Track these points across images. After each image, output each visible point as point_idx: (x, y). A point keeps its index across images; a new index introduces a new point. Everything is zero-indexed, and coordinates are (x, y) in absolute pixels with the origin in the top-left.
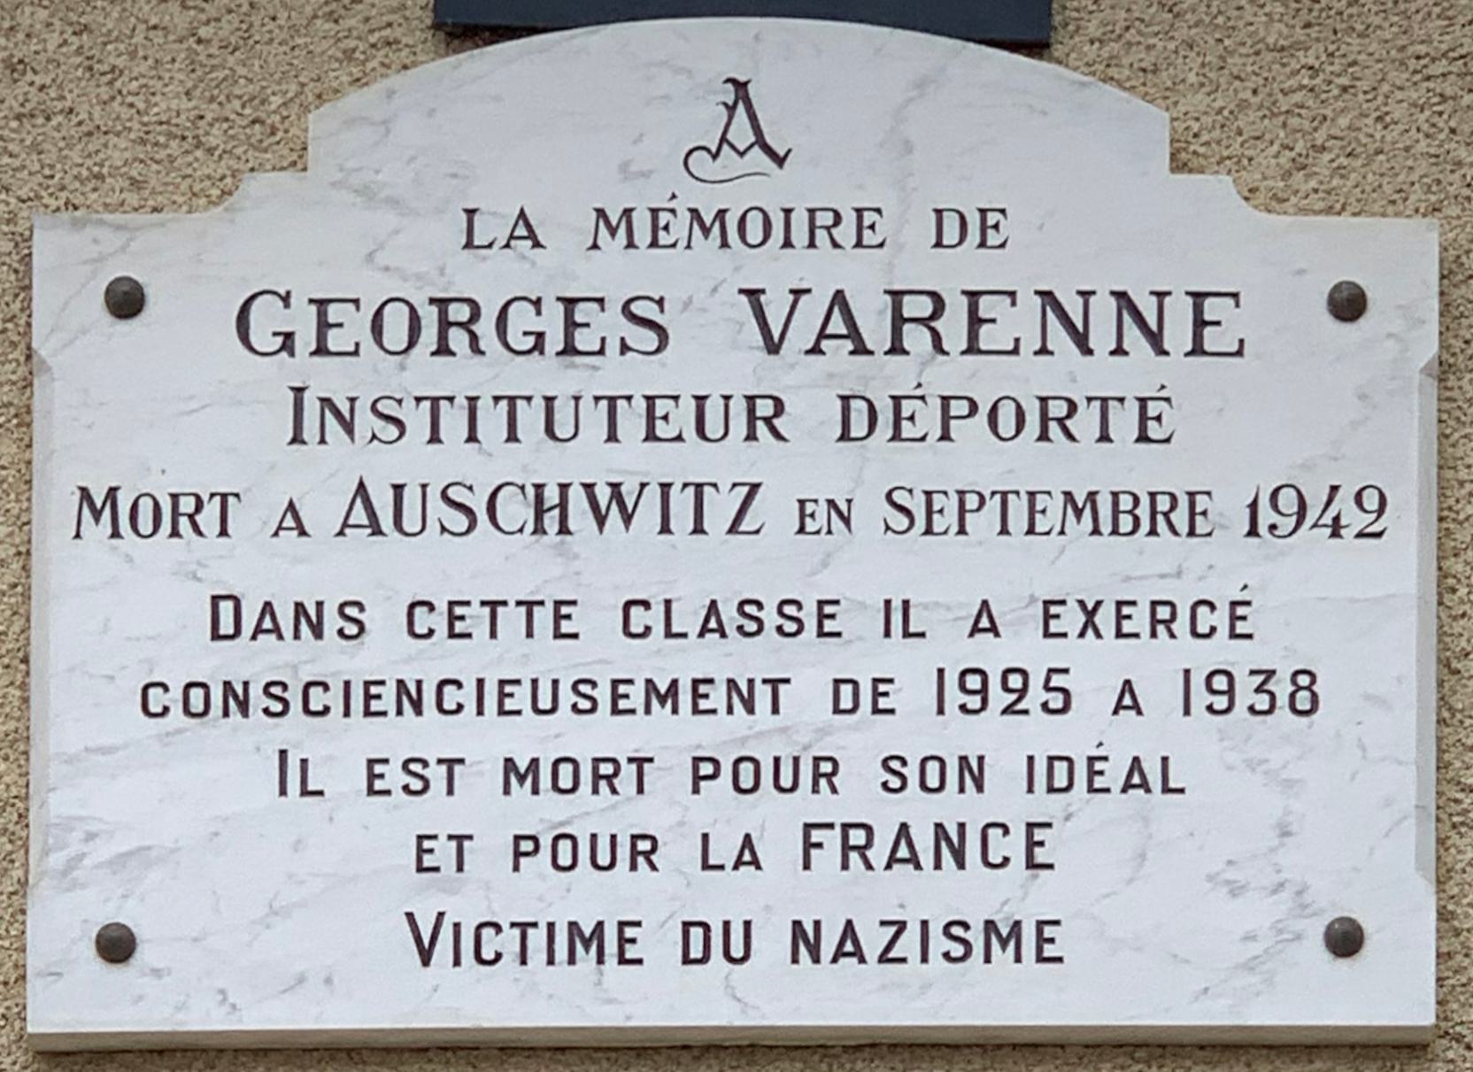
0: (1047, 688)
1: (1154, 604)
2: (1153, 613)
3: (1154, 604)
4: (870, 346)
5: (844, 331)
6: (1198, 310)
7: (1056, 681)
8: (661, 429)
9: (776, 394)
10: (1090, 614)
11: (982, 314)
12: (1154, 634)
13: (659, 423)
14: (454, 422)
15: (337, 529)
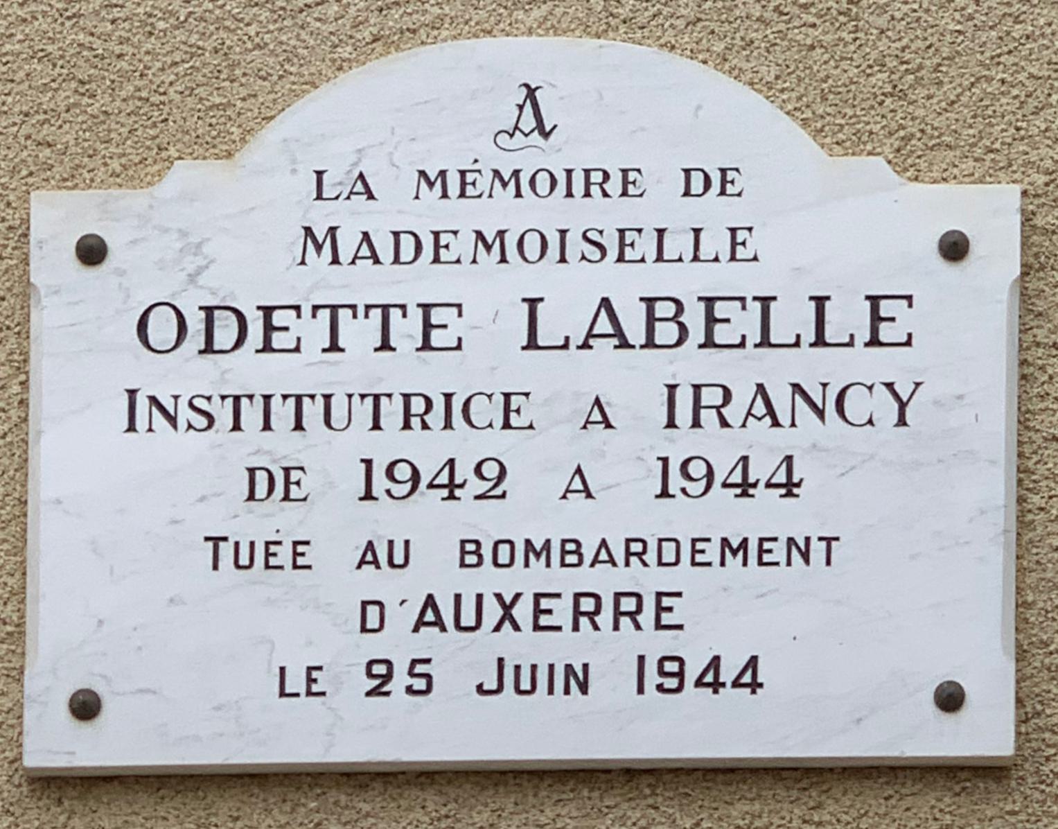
0: (411, 674)
1: (578, 596)
2: (576, 604)
3: (578, 596)
4: (631, 342)
5: (611, 331)
6: (875, 310)
7: (419, 669)
8: (514, 420)
9: (724, 383)
10: (507, 608)
11: (434, 321)
12: (576, 628)
13: (513, 415)
14: (252, 415)
15: (561, 494)
